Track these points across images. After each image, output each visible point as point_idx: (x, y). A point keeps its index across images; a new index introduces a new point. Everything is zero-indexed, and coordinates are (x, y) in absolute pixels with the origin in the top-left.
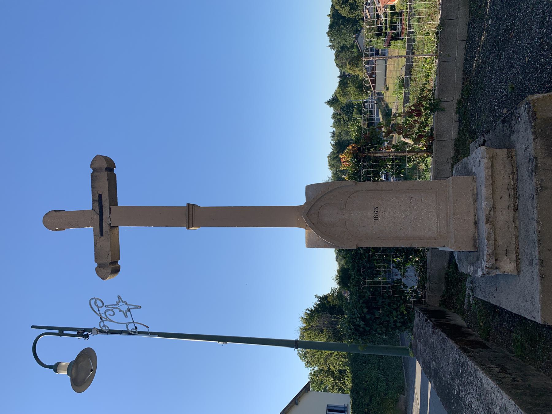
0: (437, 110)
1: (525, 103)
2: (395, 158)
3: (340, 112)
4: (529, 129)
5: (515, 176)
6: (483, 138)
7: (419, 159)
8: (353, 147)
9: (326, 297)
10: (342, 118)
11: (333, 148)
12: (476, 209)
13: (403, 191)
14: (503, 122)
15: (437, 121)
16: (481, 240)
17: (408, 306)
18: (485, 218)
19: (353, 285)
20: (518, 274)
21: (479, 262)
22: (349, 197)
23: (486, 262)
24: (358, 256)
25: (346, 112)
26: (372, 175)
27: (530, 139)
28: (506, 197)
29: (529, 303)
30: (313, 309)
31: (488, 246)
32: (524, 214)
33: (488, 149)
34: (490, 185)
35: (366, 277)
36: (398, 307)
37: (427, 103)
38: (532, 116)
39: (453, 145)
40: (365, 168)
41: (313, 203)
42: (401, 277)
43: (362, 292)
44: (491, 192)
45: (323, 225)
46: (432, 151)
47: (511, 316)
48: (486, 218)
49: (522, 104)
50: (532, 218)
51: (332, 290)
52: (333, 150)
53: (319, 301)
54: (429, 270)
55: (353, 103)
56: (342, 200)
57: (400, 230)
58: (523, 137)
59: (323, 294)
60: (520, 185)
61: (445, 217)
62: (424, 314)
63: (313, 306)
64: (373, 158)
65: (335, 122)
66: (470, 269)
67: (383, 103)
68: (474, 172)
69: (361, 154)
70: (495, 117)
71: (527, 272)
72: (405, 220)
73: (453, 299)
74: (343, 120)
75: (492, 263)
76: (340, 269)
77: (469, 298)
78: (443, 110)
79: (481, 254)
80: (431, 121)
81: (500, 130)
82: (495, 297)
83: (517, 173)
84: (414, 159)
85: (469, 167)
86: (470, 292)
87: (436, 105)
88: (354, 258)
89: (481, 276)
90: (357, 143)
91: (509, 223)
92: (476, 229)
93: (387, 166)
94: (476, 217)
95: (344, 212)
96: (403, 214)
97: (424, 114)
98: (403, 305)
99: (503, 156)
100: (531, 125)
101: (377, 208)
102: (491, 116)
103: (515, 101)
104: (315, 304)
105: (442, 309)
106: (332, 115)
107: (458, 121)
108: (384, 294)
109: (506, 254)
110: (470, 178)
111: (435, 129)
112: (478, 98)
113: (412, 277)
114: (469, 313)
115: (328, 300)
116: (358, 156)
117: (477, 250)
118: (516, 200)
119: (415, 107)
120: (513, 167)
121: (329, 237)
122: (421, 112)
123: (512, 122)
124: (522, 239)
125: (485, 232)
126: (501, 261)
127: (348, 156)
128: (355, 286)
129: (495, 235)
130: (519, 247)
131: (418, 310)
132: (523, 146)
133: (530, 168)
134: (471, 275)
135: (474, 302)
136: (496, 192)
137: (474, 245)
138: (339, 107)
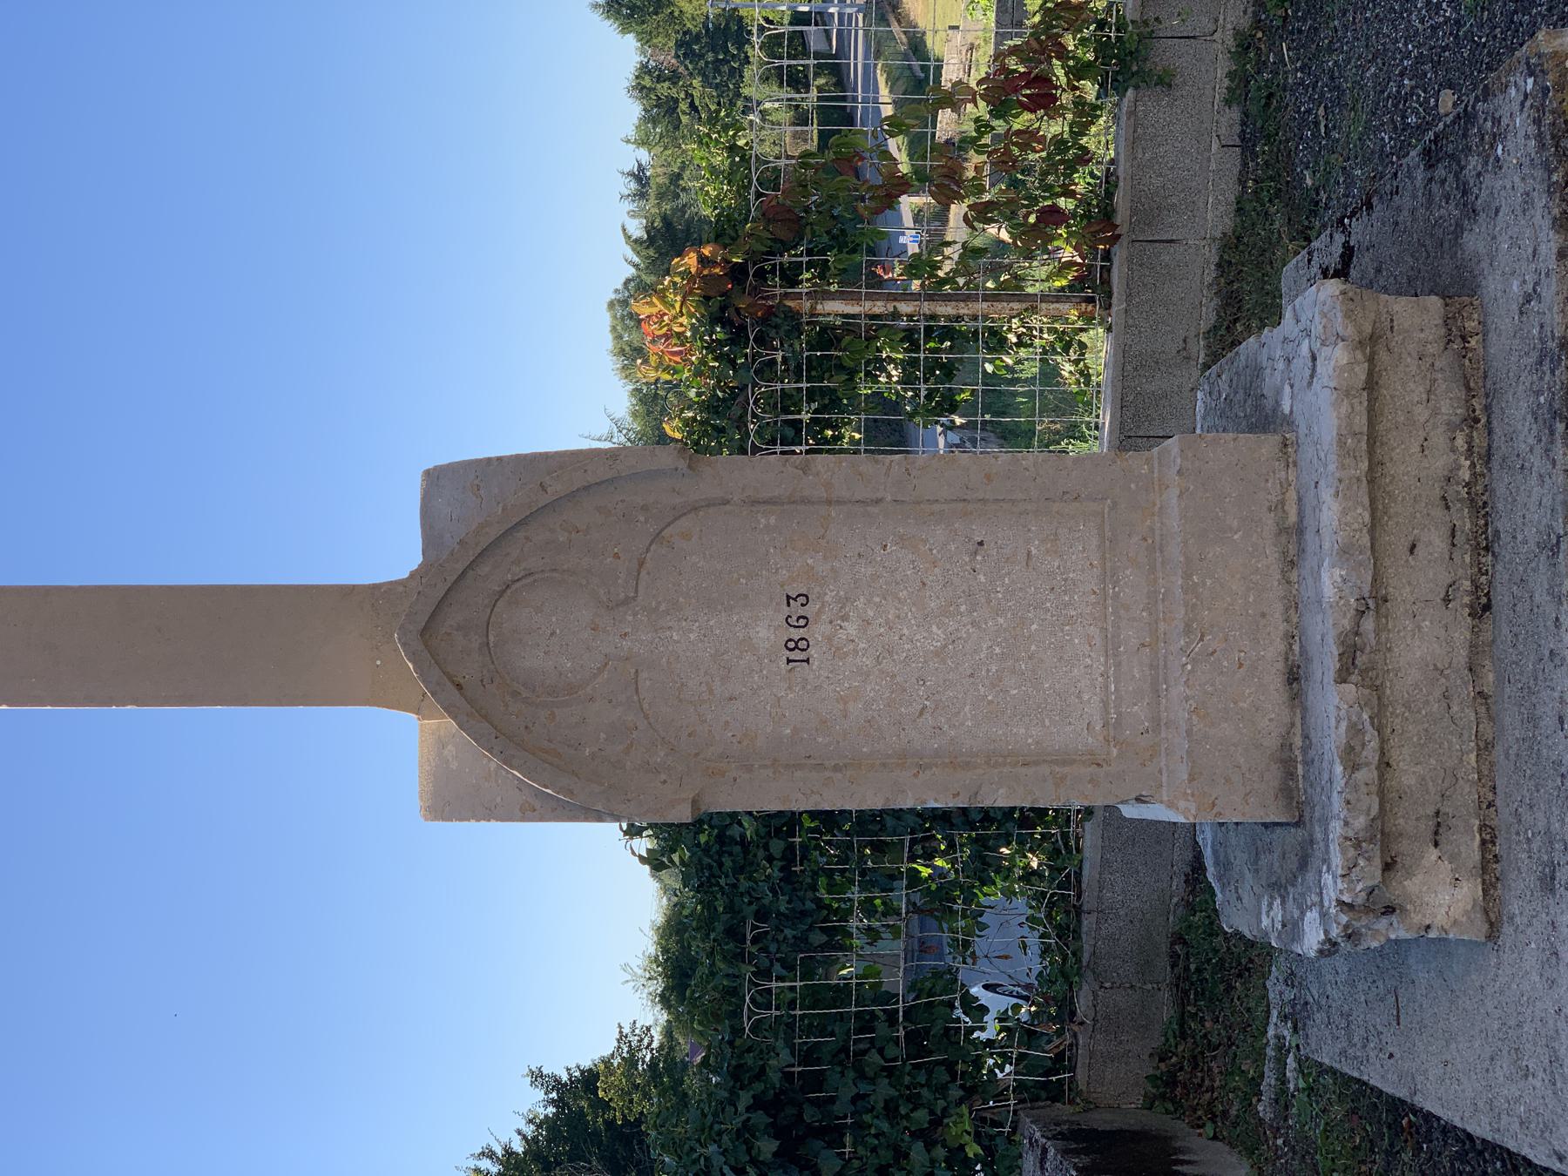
0: (1133, 81)
1: (1523, 67)
2: (922, 325)
3: (673, 61)
4: (1540, 201)
5: (1479, 440)
6: (1339, 239)
7: (1045, 336)
8: (703, 261)
9: (589, 1079)
10: (682, 95)
11: (637, 260)
12: (1293, 605)
13: (936, 507)
14: (1430, 158)
15: (1135, 137)
16: (1316, 763)
17: (988, 1116)
18: (1336, 653)
19: (705, 1012)
20: (1489, 937)
21: (1310, 876)
22: (657, 537)
23: (1339, 880)
24: (731, 854)
25: (707, 63)
26: (805, 417)
27: (1543, 249)
28: (1435, 541)
29: (1538, 1084)
30: (518, 1147)
31: (1349, 797)
32: (1515, 629)
33: (1350, 294)
34: (1358, 479)
35: (772, 965)
36: (937, 1122)
37: (1083, 42)
38: (1553, 137)
39: (1213, 267)
40: (767, 374)
41: (460, 567)
42: (954, 958)
43: (749, 1050)
44: (1367, 518)
45: (515, 694)
46: (1110, 295)
47: (1467, 1147)
48: (1341, 651)
49: (1509, 72)
50: (1551, 651)
51: (622, 1037)
52: (636, 266)
53: (553, 1102)
54: (1093, 918)
55: (741, 18)
56: (616, 556)
57: (921, 714)
58: (1514, 242)
59: (572, 1065)
60: (1502, 483)
61: (1143, 645)
62: (1066, 1152)
63: (519, 1132)
64: (808, 323)
65: (649, 119)
66: (1272, 913)
67: (895, 28)
68: (1287, 411)
69: (749, 300)
70: (1404, 130)
71: (1530, 924)
72: (944, 661)
73: (1210, 1069)
74: (692, 106)
75: (1370, 883)
76: (668, 921)
77: (1281, 1063)
78: (1165, 81)
79: (1319, 836)
80: (1100, 140)
81: (1414, 197)
82: (1391, 1056)
83: (1489, 422)
84: (1019, 337)
85: (1270, 382)
86: (1286, 1033)
87: (1131, 53)
88: (710, 867)
89: (1321, 952)
90: (727, 241)
91: (1447, 678)
92: (1292, 707)
93: (882, 369)
94: (1296, 648)
95: (630, 618)
96: (934, 628)
97: (1066, 98)
98: (964, 1109)
99: (1422, 335)
100: (1549, 178)
101: (802, 600)
102: (1382, 125)
103: (1490, 54)
104: (530, 1121)
105: (1157, 1121)
106: (632, 77)
107: (1238, 142)
108: (865, 1052)
109: (1436, 833)
110: (1268, 444)
111: (1125, 179)
112: (1328, 28)
113: (1006, 957)
114: (1280, 1142)
115: (601, 1094)
116: (732, 310)
117: (1301, 816)
118: (1483, 560)
119: (1022, 61)
120: (1469, 389)
121: (544, 761)
122: (1056, 88)
123: (1468, 162)
124: (1507, 756)
125: (1333, 722)
126: (1409, 875)
127: (678, 306)
128: (717, 1018)
129: (1383, 741)
130: (1498, 802)
131: (1038, 1135)
132: (1515, 288)
133: (1542, 399)
134: (1274, 944)
135: (1302, 1084)
136: (1390, 518)
137: (1287, 792)
138: (668, 35)
